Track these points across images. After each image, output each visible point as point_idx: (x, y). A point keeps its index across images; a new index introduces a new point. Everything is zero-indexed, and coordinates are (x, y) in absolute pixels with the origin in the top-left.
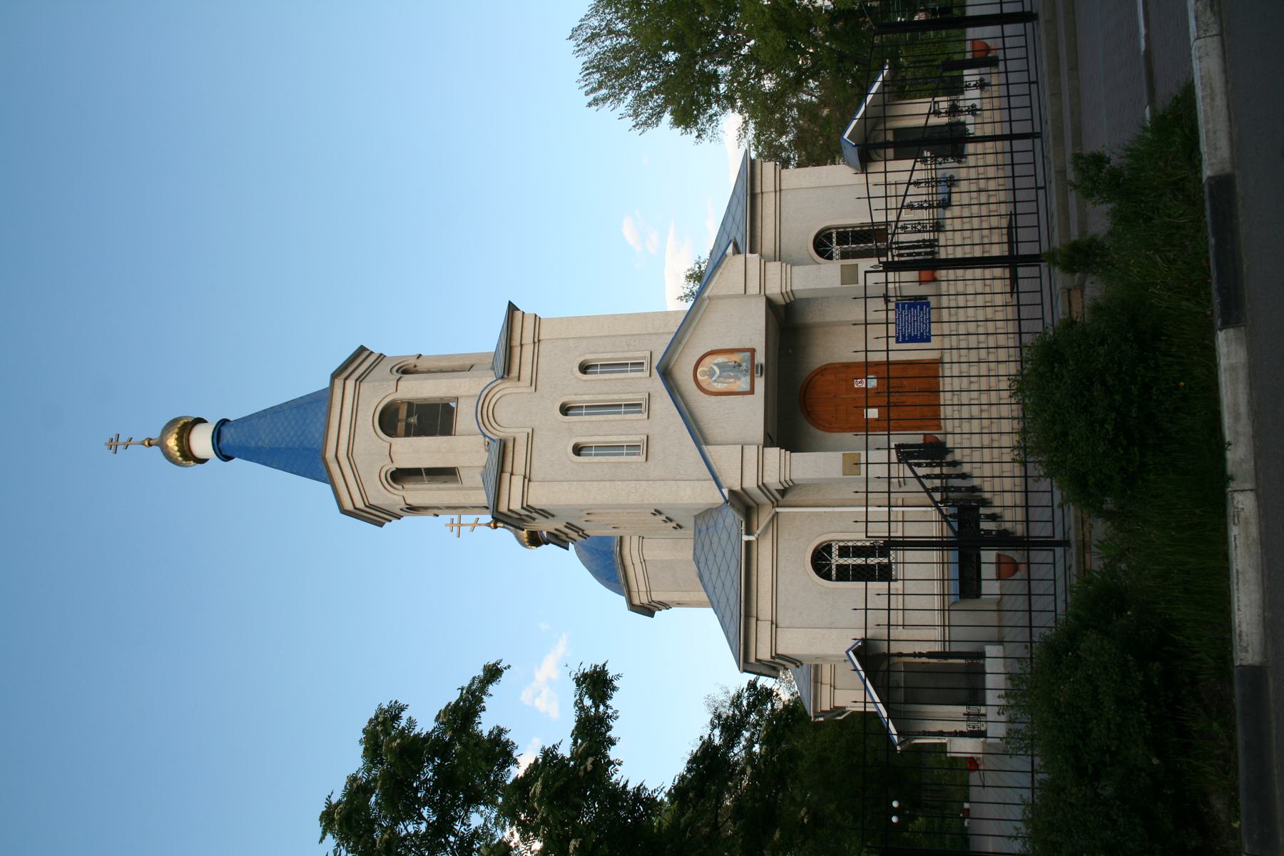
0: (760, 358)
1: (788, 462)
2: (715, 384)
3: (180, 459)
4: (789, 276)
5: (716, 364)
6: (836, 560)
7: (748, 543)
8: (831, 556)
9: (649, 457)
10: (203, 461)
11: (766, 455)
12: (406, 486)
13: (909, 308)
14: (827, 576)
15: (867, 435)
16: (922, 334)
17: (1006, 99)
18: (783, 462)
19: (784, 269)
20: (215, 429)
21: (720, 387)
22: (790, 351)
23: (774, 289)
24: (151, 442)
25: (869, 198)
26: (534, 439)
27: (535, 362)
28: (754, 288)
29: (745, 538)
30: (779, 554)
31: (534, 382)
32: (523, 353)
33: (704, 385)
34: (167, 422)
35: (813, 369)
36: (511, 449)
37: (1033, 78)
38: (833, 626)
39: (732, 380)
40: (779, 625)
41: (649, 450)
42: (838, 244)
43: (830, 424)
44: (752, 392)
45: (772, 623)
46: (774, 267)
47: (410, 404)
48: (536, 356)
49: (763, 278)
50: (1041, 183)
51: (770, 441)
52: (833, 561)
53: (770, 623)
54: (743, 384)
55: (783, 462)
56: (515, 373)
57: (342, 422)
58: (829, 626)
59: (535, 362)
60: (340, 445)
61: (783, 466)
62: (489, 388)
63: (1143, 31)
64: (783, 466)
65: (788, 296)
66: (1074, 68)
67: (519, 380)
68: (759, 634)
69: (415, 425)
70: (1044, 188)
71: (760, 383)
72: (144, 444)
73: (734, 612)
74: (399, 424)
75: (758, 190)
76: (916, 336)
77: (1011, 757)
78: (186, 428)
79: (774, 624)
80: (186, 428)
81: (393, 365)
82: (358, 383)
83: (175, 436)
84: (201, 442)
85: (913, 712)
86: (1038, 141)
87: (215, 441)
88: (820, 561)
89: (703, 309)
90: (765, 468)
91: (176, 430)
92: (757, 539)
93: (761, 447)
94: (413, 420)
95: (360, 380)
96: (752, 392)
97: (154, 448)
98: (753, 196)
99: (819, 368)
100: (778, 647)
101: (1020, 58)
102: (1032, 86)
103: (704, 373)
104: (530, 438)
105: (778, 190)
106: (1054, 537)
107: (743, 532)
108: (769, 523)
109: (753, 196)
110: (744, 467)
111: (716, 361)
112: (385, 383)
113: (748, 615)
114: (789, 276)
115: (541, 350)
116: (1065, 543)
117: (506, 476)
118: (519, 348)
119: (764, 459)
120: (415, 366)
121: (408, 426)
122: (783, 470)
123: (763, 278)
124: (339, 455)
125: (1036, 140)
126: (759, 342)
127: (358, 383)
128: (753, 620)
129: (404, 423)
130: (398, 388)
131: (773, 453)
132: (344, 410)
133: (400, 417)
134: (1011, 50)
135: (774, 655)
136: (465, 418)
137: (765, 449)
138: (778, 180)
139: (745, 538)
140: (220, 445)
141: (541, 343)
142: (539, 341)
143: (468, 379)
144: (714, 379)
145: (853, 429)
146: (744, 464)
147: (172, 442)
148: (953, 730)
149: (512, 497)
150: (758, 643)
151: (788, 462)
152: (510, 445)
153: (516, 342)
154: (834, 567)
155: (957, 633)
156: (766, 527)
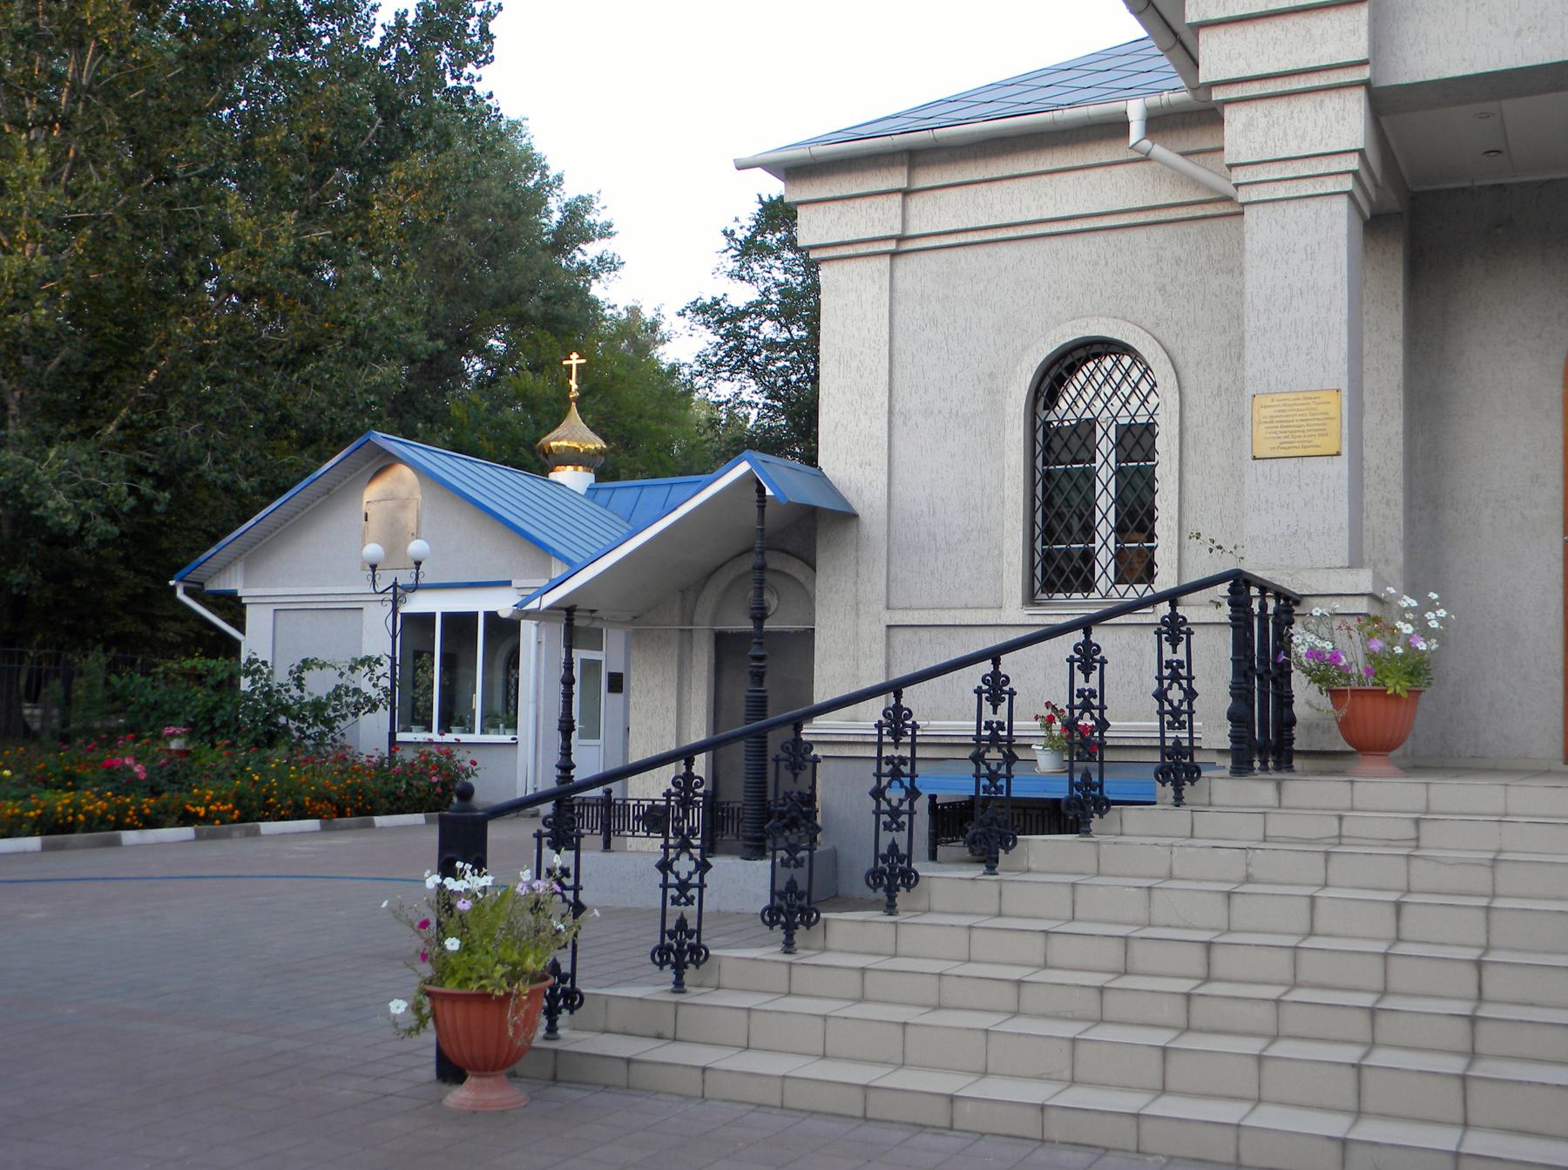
11: (1332, 101)
29: (1135, 112)
30: (1113, 236)
38: (898, 421)
40: (901, 262)
45: (900, 239)
53: (897, 231)
58: (897, 407)
61: (1289, 170)
64: (1289, 170)
65: (1043, 821)
68: (865, 203)
77: (874, 775)
79: (899, 247)
85: (692, 650)
90: (1280, 108)
93: (1364, 73)
100: (836, 266)
107: (1154, 100)
108: (1212, 190)
110: (1278, 21)
119: (1319, 97)
128: (898, 179)
135: (814, 255)
137: (1361, 93)
145: (443, 847)
146: (1289, 22)
150: (837, 206)
156: (1196, 183)
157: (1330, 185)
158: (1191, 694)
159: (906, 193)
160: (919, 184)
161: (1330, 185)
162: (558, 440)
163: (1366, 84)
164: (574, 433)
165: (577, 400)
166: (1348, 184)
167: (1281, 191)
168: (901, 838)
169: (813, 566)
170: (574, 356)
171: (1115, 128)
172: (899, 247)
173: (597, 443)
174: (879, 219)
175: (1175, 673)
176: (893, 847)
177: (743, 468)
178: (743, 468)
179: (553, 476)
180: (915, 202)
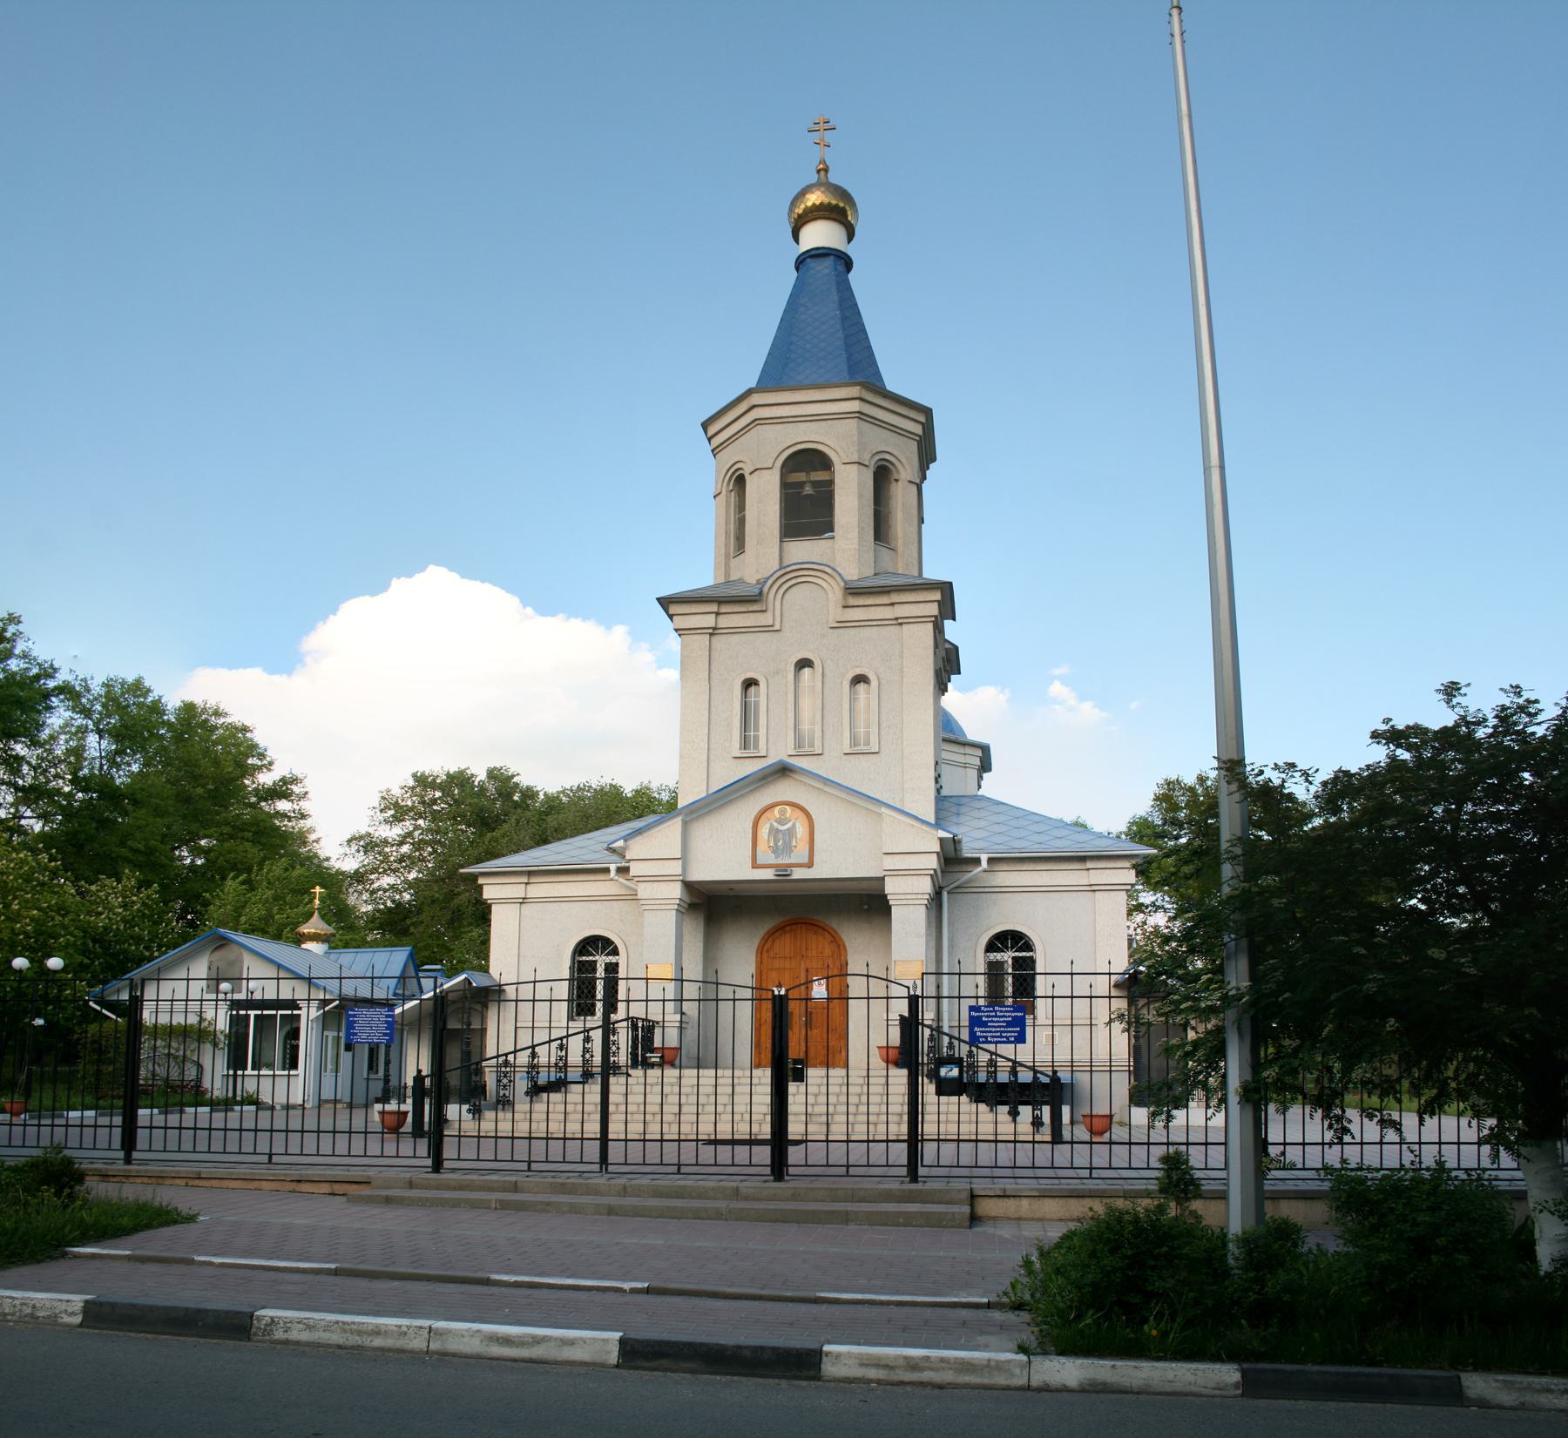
0: (798, 874)
1: (663, 907)
2: (768, 826)
3: (803, 206)
4: (910, 902)
5: (794, 825)
6: (601, 961)
7: (607, 870)
8: (608, 955)
9: (738, 760)
10: (796, 238)
12: (733, 493)
13: (386, 1022)
14: (991, 947)
15: (753, 988)
16: (355, 1034)
17: (269, 1128)
18: (662, 902)
19: (920, 896)
20: (840, 251)
21: (764, 832)
22: (866, 907)
23: (891, 887)
24: (822, 173)
25: (535, 982)
26: (766, 634)
27: (870, 623)
28: (891, 863)
29: (984, 858)
31: (842, 625)
32: (882, 608)
33: (767, 814)
34: (846, 188)
35: (839, 932)
36: (751, 609)
37: (275, 1159)
39: (772, 844)
40: (523, 905)
41: (747, 760)
42: (1013, 958)
43: (767, 951)
44: (755, 866)
46: (925, 886)
47: (831, 483)
48: (879, 623)
49: (907, 873)
50: (684, 1170)
51: (689, 886)
52: (597, 958)
54: (765, 856)
55: (662, 902)
56: (852, 601)
57: (802, 405)
59: (870, 623)
60: (770, 408)
61: (658, 902)
62: (834, 574)
63: (627, 1286)
64: (658, 902)
66: (663, 1214)
67: (845, 607)
69: (799, 493)
70: (529, 1169)
71: (768, 874)
72: (820, 163)
73: (576, 859)
74: (804, 474)
75: (1089, 865)
76: (354, 1028)
78: (839, 211)
79: (524, 901)
80: (839, 211)
81: (895, 453)
82: (857, 415)
83: (826, 200)
84: (819, 234)
86: (596, 1167)
87: (813, 253)
88: (593, 944)
89: (868, 807)
91: (834, 202)
92: (612, 880)
93: (681, 878)
94: (808, 490)
95: (861, 416)
96: (755, 866)
97: (817, 176)
98: (1083, 859)
99: (840, 938)
101: (1479, 1155)
102: (267, 1157)
103: (783, 812)
104: (768, 629)
105: (1093, 889)
106: (922, 1166)
107: (619, 865)
109: (1083, 859)
111: (798, 825)
112: (856, 448)
113: (530, 874)
114: (910, 902)
115: (889, 628)
116: (913, 1175)
117: (714, 608)
118: (888, 602)
120: (897, 481)
121: (801, 484)
122: (653, 902)
123: (907, 873)
124: (755, 410)
125: (769, 1168)
126: (821, 871)
127: (857, 415)
129: (804, 479)
130: (848, 466)
131: (676, 891)
132: (818, 405)
133: (813, 474)
134: (36, 1134)
136: (803, 550)
138: (1110, 888)
139: (984, 858)
140: (808, 260)
141: (898, 627)
142: (901, 624)
143: (857, 546)
144: (775, 824)
147: (814, 198)
148: (391, 1072)
149: (688, 617)
151: (663, 907)
152: (755, 607)
153: (895, 598)
154: (591, 958)
155: (1101, 1081)
157: (670, 907)
158: (618, 1048)
159: (526, 884)
160: (723, 610)
161: (670, 907)
162: (306, 929)
163: (682, 881)
164: (314, 925)
165: (318, 909)
166: (676, 907)
167: (655, 907)
168: (507, 1093)
169: (487, 1008)
170: (318, 887)
171: (607, 870)
172: (524, 901)
173: (330, 930)
174: (516, 891)
175: (586, 1051)
176: (504, 1095)
177: (463, 977)
178: (463, 977)
179: (303, 946)
180: (529, 887)
